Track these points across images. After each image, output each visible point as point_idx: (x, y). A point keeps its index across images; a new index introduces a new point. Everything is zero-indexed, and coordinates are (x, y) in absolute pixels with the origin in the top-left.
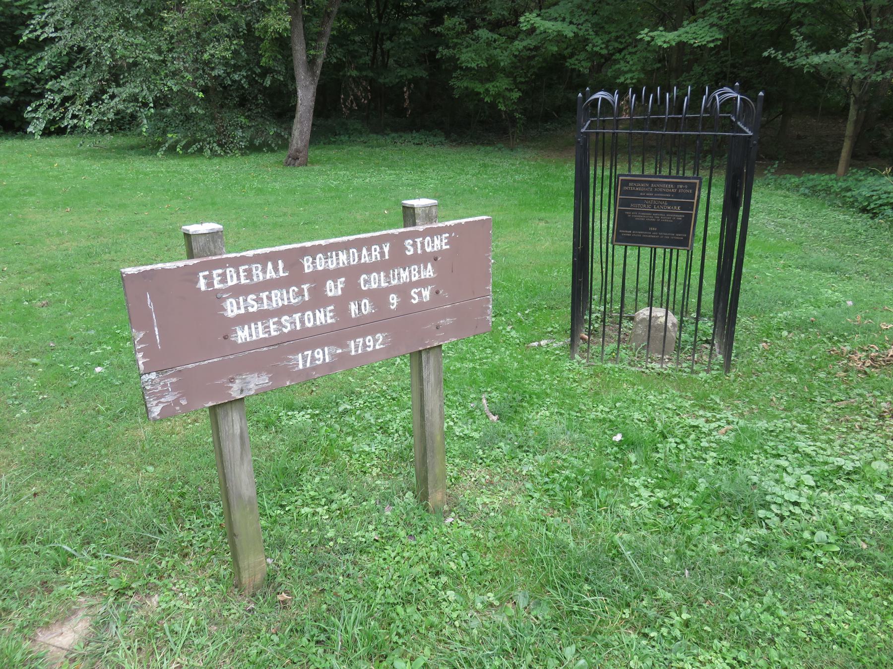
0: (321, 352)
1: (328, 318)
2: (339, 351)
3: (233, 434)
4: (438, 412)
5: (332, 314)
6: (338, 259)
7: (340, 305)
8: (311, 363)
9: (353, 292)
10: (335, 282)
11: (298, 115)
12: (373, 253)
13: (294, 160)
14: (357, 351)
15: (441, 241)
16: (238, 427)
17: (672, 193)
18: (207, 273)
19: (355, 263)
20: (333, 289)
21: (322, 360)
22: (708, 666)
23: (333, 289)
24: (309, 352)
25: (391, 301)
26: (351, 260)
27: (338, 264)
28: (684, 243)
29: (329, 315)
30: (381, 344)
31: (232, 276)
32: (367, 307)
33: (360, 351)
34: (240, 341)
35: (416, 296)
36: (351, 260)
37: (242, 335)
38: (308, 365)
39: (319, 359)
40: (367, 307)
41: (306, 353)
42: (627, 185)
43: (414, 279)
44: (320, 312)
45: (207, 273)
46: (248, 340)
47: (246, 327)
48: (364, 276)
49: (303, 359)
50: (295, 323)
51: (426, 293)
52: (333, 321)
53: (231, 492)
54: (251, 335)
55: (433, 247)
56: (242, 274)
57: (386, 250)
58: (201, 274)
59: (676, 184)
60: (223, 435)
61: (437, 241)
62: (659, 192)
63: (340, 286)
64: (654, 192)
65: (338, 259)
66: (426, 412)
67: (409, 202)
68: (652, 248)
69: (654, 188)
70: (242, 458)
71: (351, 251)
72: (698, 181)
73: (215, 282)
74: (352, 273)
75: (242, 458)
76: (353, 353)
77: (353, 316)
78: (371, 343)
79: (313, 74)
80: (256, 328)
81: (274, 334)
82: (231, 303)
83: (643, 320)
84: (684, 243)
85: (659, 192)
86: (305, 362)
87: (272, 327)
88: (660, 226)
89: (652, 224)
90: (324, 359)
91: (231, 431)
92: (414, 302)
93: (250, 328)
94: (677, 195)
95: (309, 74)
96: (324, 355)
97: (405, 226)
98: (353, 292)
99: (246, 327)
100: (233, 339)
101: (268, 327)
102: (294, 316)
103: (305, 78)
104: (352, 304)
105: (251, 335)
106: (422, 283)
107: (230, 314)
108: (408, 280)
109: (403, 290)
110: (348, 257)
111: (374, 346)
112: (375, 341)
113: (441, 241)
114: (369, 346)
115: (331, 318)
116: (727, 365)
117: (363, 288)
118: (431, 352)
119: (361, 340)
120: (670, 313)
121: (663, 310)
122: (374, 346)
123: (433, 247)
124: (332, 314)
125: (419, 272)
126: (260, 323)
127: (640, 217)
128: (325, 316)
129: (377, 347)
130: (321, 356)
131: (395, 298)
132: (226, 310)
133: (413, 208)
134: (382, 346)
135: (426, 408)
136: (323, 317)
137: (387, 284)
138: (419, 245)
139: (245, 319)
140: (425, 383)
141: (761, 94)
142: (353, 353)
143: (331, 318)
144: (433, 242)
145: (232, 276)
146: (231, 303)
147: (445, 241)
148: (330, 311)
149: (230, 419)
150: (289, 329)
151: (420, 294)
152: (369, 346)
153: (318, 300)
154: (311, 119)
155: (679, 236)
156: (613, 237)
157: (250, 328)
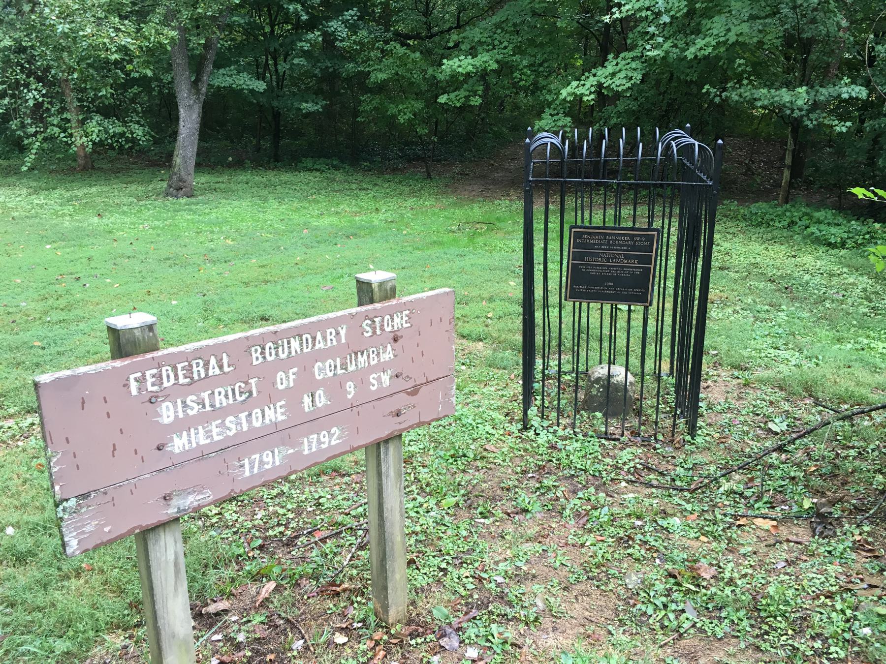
0: (270, 454)
1: (279, 415)
2: (291, 451)
3: (167, 562)
4: (398, 509)
5: (283, 410)
6: (289, 347)
7: (293, 396)
8: (259, 467)
9: (307, 384)
10: (286, 373)
11: (180, 138)
12: (329, 338)
13: (179, 189)
14: (310, 449)
15: (402, 318)
16: (173, 552)
17: (628, 246)
18: (139, 374)
19: (309, 350)
20: (284, 380)
21: (271, 463)
22: (552, 663)
23: (284, 380)
24: (257, 456)
25: (348, 389)
26: (305, 346)
27: (290, 353)
28: (643, 298)
29: (279, 410)
30: (338, 438)
31: (168, 376)
32: (322, 400)
33: (314, 450)
34: (177, 451)
35: (375, 382)
36: (305, 346)
37: (179, 444)
38: (256, 471)
39: (268, 463)
40: (322, 400)
41: (253, 457)
42: (581, 238)
43: (372, 363)
44: (269, 408)
45: (139, 374)
46: (187, 448)
47: (185, 433)
48: (319, 364)
49: (250, 464)
50: (241, 424)
51: (386, 379)
52: (284, 417)
53: (163, 632)
54: (190, 442)
55: (393, 326)
56: (180, 374)
57: (343, 332)
58: (132, 377)
59: (632, 236)
60: (153, 563)
61: (397, 320)
62: (615, 245)
63: (292, 377)
64: (609, 244)
65: (289, 347)
66: (385, 510)
67: (365, 276)
68: (612, 305)
69: (609, 240)
70: (176, 590)
71: (304, 337)
72: (655, 233)
73: (149, 384)
74: (305, 363)
75: (176, 590)
76: (306, 452)
77: (307, 410)
78: (326, 439)
79: (198, 92)
80: (197, 434)
81: (217, 438)
82: (167, 407)
83: (598, 380)
84: (643, 298)
85: (615, 245)
86: (252, 468)
87: (215, 431)
88: (618, 281)
89: (609, 279)
90: (274, 462)
91: (163, 558)
92: (373, 388)
93: (189, 435)
94: (634, 248)
95: (193, 91)
96: (273, 457)
97: (360, 304)
98: (307, 384)
99: (185, 433)
100: (169, 449)
101: (211, 431)
102: (240, 415)
103: (189, 96)
104: (305, 396)
105: (190, 442)
106: (382, 368)
107: (166, 421)
108: (367, 364)
109: (361, 379)
110: (301, 344)
111: (330, 441)
112: (331, 436)
113: (402, 318)
114: (324, 443)
115: (282, 414)
116: (692, 429)
117: (318, 377)
118: (391, 442)
119: (315, 436)
120: (629, 373)
121: (623, 370)
122: (330, 441)
123: (393, 326)
124: (283, 410)
125: (378, 355)
126: (200, 428)
127: (593, 272)
128: (276, 413)
129: (333, 443)
130: (270, 459)
131: (353, 386)
132: (161, 416)
133: (369, 284)
134: (338, 441)
135: (385, 506)
136: (275, 414)
137: (344, 371)
138: (378, 325)
139: (183, 425)
140: (384, 478)
141: (688, 125)
142: (306, 452)
143: (282, 414)
144: (393, 319)
145: (168, 376)
146: (167, 407)
147: (405, 318)
148: (281, 407)
149: (162, 543)
150: (234, 431)
151: (379, 379)
152: (324, 443)
153: (270, 397)
154: (196, 142)
155: (638, 291)
156: (566, 293)
157: (189, 435)
